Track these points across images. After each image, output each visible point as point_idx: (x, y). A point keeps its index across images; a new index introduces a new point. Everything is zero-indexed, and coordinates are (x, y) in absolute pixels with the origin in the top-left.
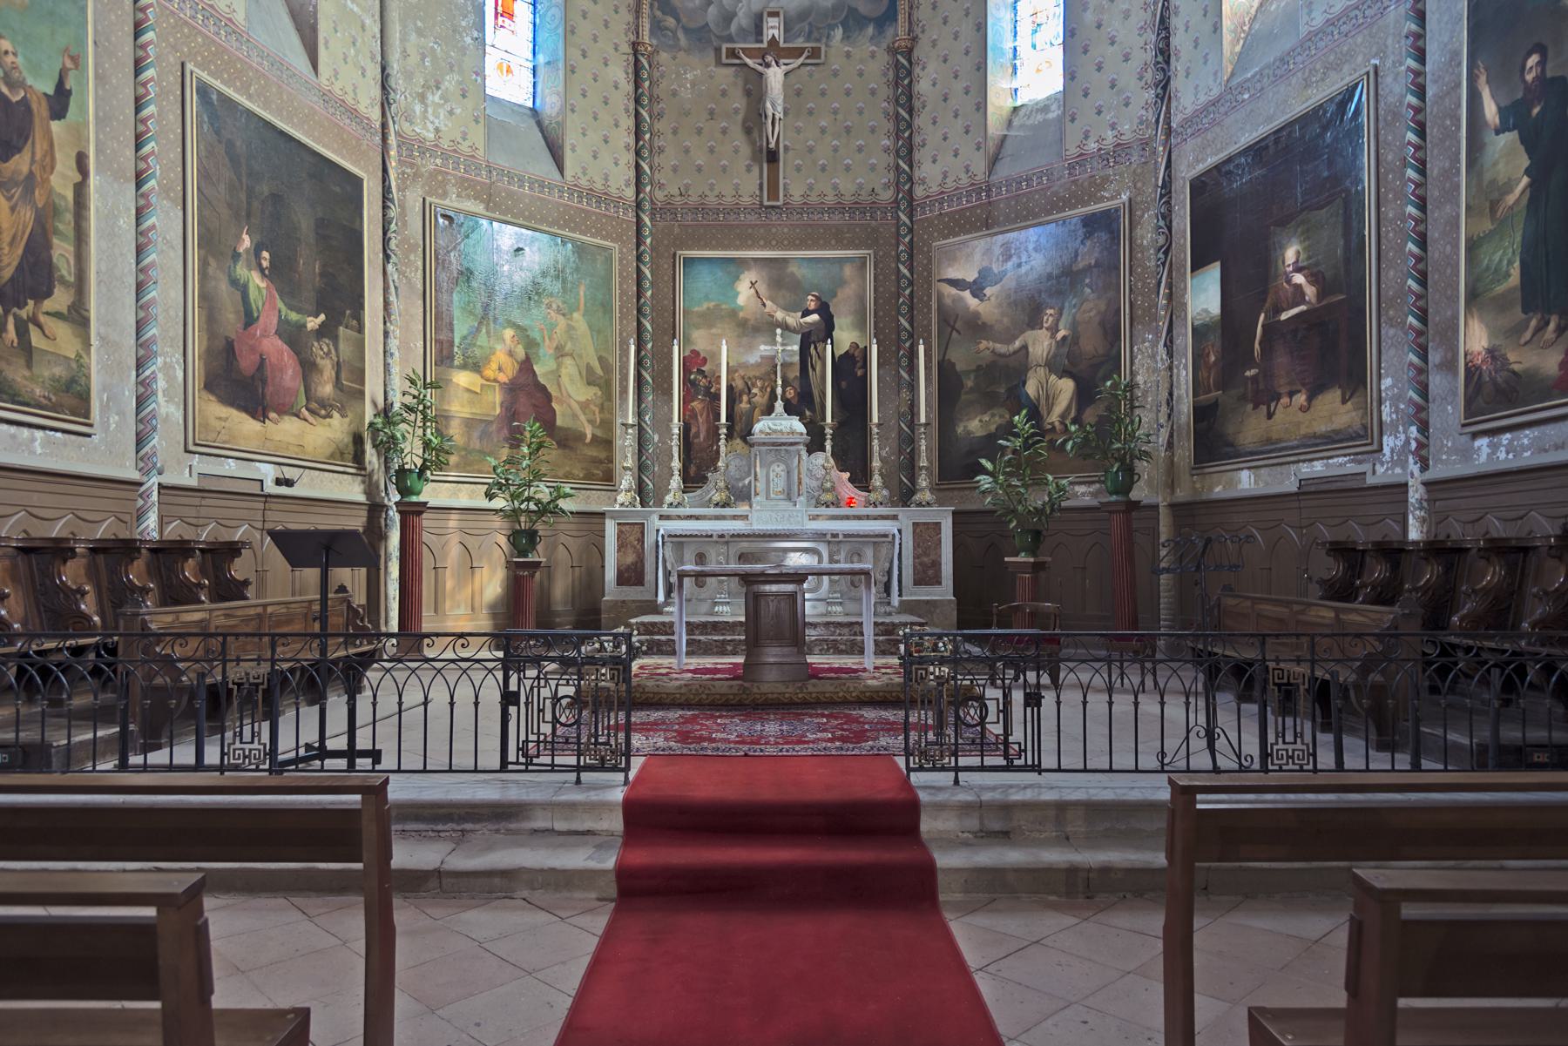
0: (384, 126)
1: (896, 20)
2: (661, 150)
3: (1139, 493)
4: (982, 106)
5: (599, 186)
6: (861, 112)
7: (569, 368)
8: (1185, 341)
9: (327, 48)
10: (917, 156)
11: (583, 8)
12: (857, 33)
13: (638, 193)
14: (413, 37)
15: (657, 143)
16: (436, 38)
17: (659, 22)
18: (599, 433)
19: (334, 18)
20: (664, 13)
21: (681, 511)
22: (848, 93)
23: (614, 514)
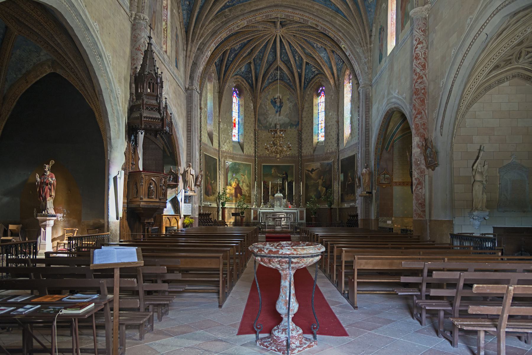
0: (219, 150)
2: (259, 147)
3: (333, 206)
4: (312, 142)
5: (249, 154)
6: (293, 141)
7: (244, 185)
8: (340, 183)
10: (302, 148)
13: (255, 154)
14: (223, 135)
15: (258, 146)
18: (249, 195)
21: (263, 208)
22: (291, 137)
23: (253, 209)
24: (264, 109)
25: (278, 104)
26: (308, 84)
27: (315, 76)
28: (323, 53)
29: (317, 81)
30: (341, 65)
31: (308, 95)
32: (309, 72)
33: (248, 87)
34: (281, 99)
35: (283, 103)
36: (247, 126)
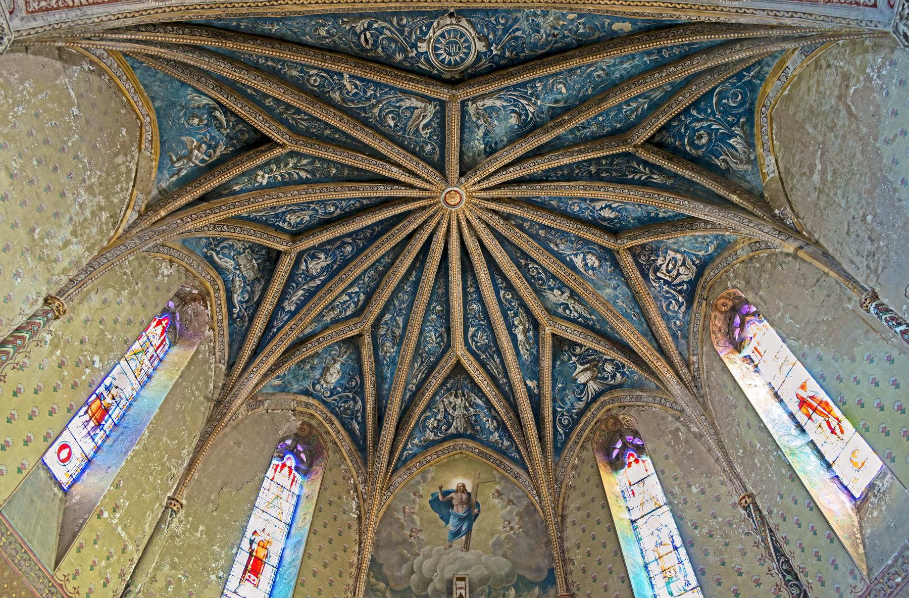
1: (555, 583)
9: (79, 551)
11: (314, 569)
12: (526, 593)
14: (167, 568)
16: (185, 572)
17: (373, 586)
19: (99, 533)
20: (377, 579)
24: (402, 527)
25: (460, 511)
26: (568, 435)
27: (588, 405)
28: (609, 286)
29: (598, 416)
30: (680, 316)
31: (575, 467)
32: (564, 389)
33: (346, 445)
34: (469, 494)
35: (478, 504)
36: (315, 574)
